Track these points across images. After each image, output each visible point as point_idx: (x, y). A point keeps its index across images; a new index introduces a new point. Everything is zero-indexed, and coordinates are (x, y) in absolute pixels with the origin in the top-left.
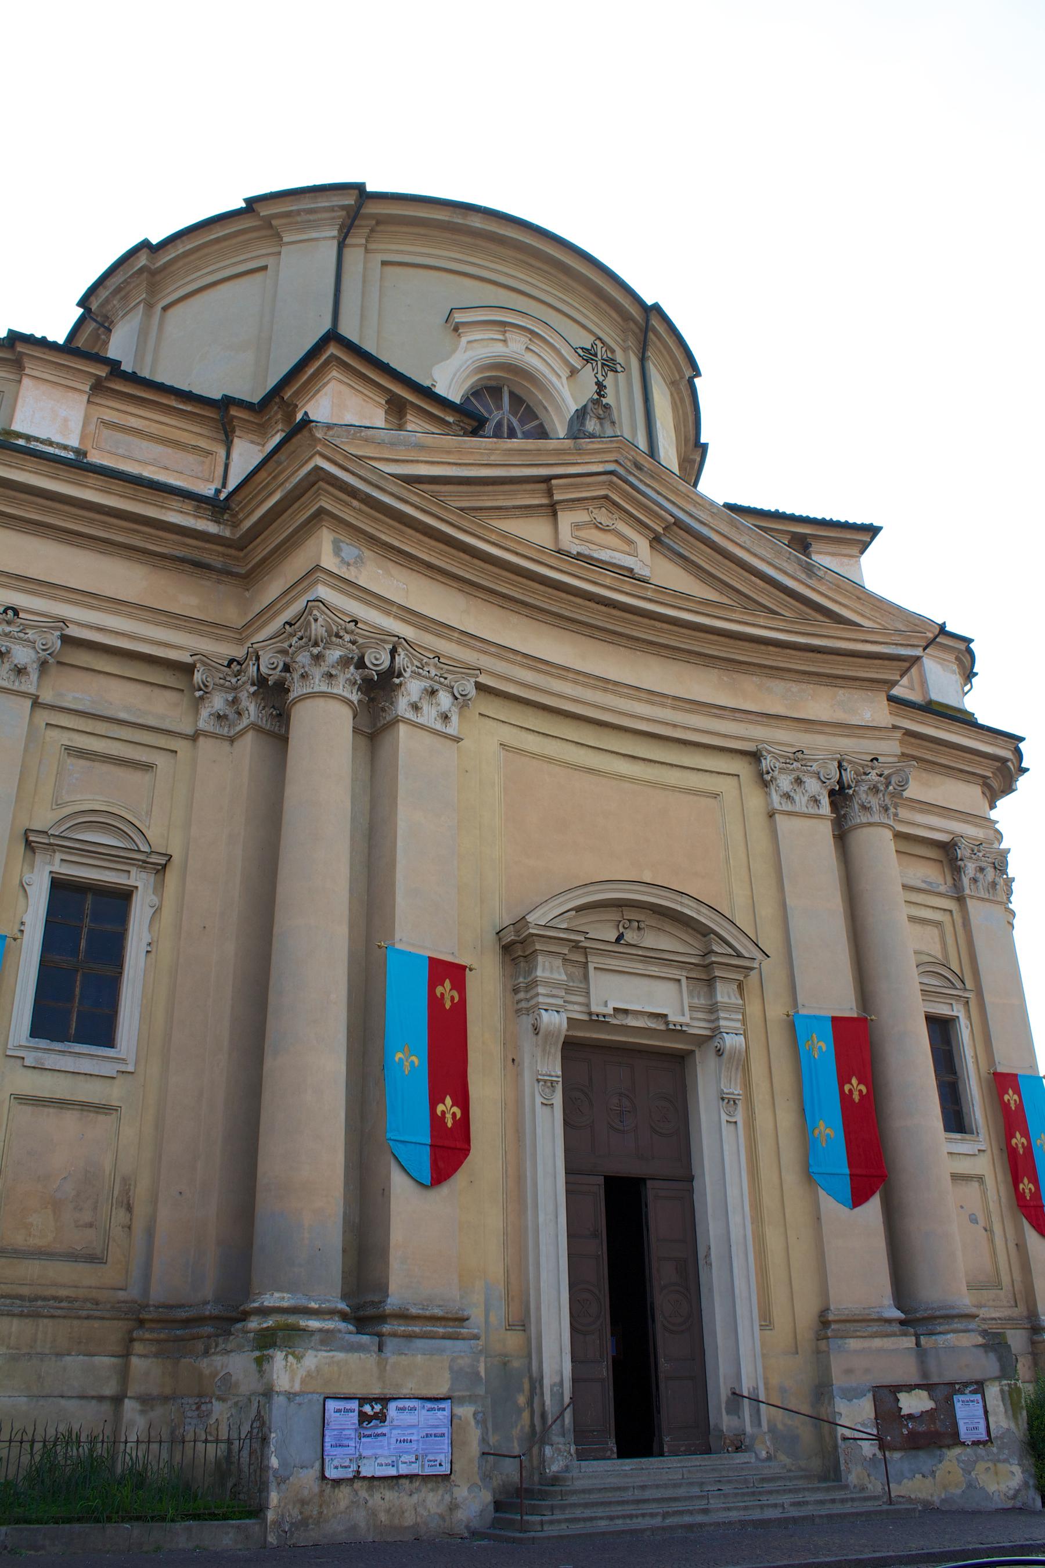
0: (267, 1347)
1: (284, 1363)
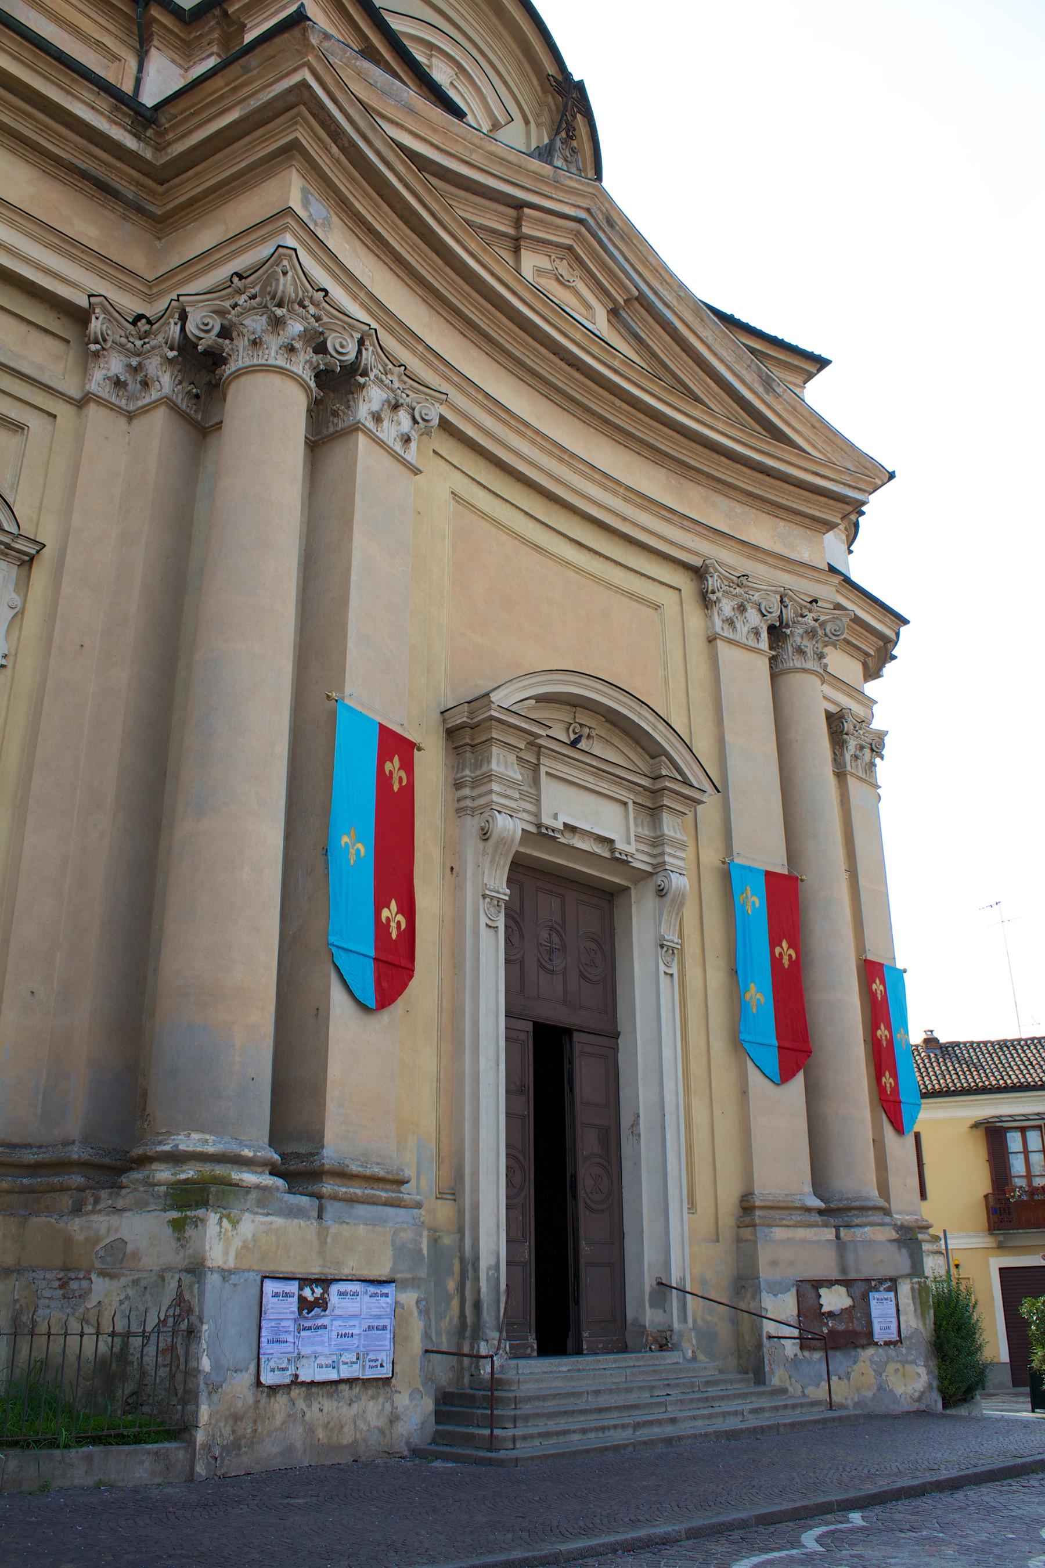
0: (190, 1206)
1: (217, 1228)
